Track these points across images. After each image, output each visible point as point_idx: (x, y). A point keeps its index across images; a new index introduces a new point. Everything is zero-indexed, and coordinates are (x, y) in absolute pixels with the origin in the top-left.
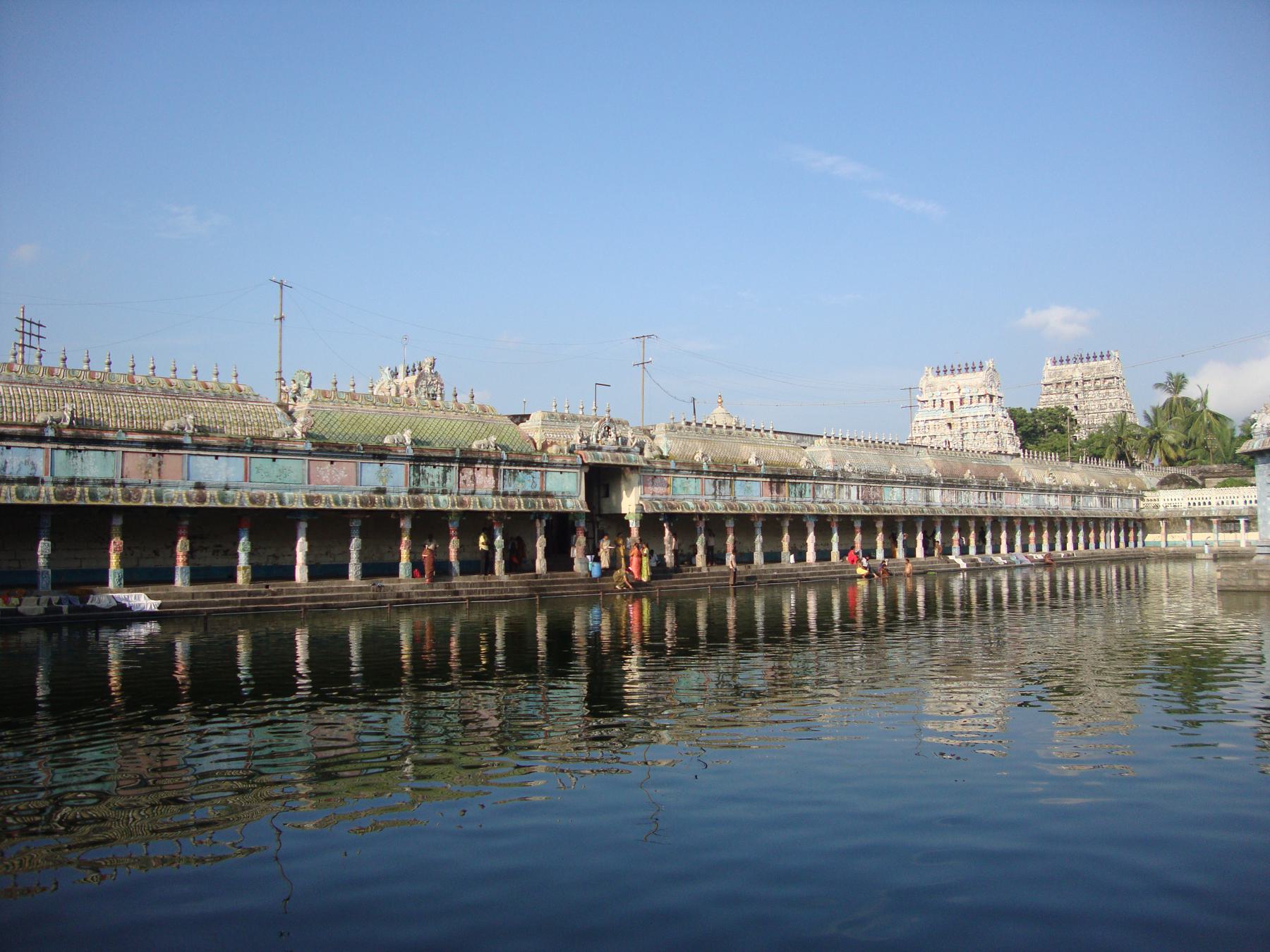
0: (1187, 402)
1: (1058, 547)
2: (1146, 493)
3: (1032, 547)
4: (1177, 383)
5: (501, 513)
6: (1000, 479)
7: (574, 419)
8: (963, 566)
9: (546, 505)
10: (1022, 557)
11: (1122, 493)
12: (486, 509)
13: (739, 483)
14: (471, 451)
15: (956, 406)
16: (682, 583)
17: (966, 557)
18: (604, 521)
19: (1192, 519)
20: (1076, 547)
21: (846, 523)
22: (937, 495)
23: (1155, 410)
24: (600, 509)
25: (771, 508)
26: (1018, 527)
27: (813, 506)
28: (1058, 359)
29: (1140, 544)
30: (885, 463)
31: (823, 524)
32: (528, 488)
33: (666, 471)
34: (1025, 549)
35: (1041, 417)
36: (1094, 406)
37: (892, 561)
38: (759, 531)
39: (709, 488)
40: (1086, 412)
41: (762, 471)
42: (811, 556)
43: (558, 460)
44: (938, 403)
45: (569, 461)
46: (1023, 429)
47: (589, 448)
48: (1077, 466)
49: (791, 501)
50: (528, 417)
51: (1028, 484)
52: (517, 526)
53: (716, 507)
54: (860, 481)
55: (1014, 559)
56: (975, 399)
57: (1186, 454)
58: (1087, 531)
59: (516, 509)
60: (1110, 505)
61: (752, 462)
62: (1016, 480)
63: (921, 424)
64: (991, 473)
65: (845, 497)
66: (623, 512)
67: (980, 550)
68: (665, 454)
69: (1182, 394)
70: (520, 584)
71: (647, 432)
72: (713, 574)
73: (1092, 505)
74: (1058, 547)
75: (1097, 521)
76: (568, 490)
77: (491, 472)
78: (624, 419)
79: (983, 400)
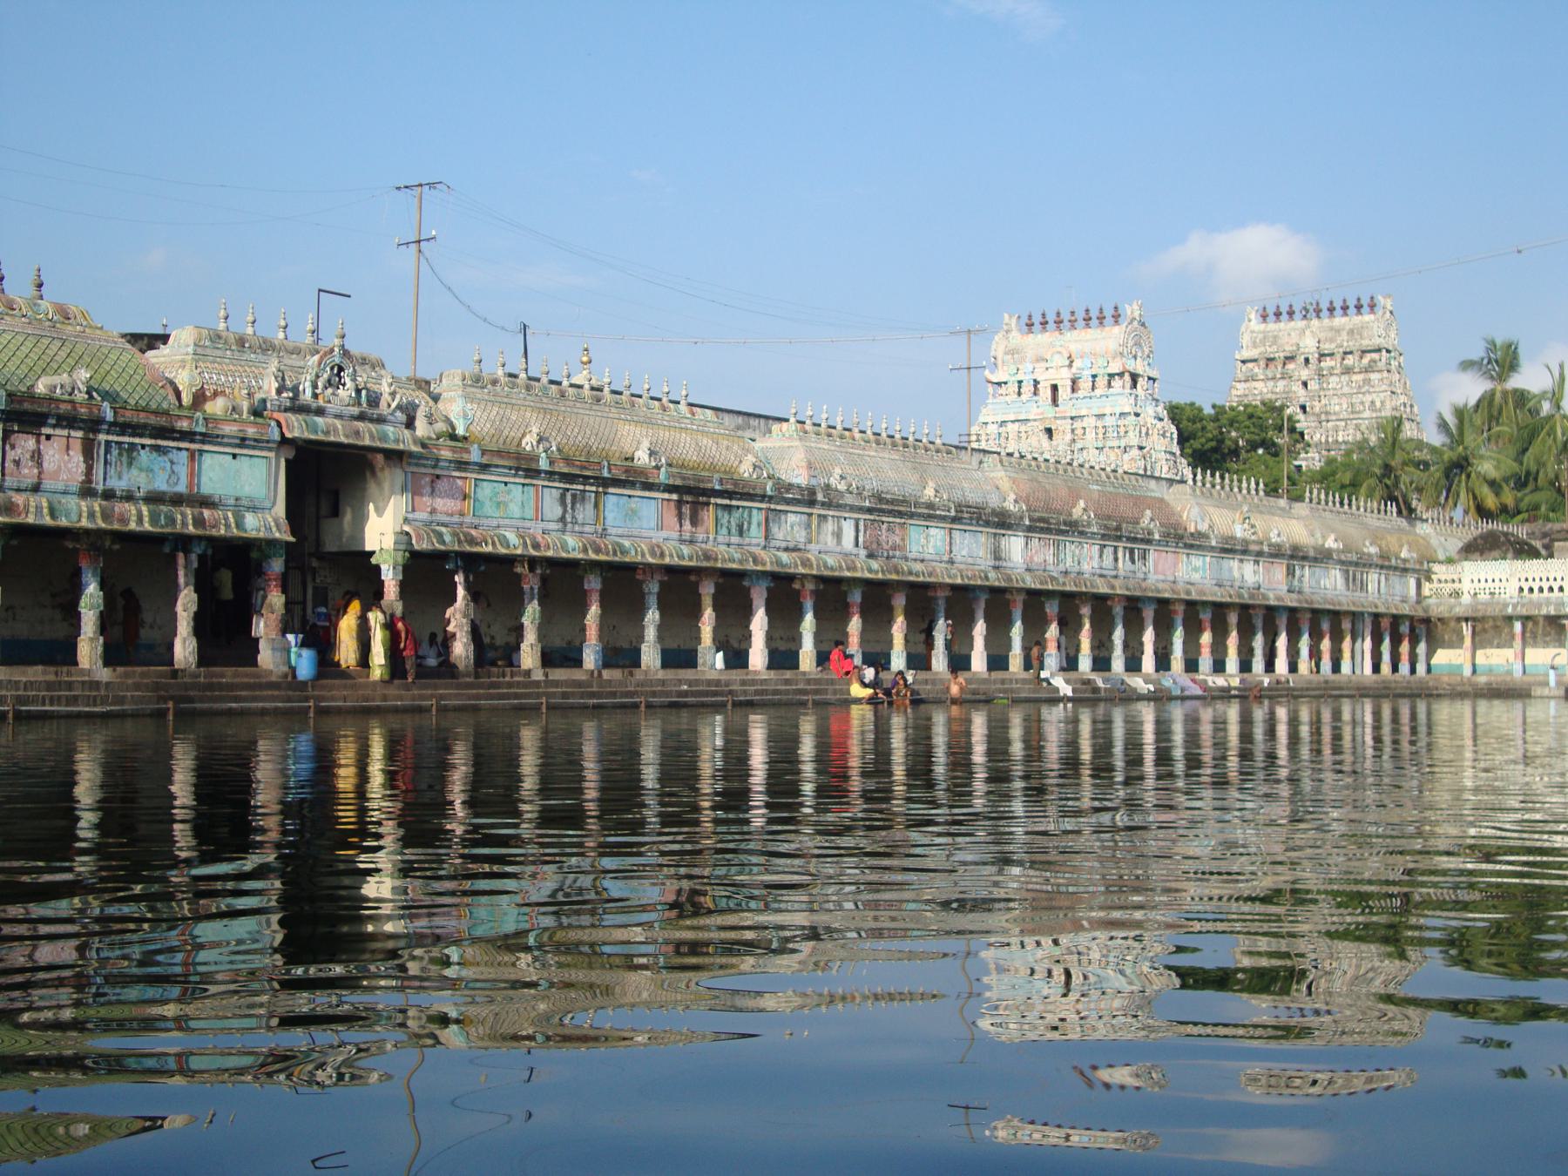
0: (1521, 397)
1: (1258, 664)
2: (1436, 567)
3: (1205, 662)
4: (1504, 360)
5: (100, 533)
6: (1145, 521)
7: (267, 347)
8: (1066, 690)
9: (199, 522)
10: (1185, 680)
11: (1388, 564)
12: (63, 522)
13: (614, 503)
14: (31, 396)
15: (1064, 393)
16: (492, 697)
17: (1072, 675)
18: (326, 572)
19: (1526, 619)
20: (1293, 668)
21: (833, 594)
22: (1016, 548)
23: (1460, 413)
24: (318, 542)
25: (678, 553)
26: (1179, 619)
27: (763, 554)
28: (1271, 311)
29: (1421, 668)
30: (913, 478)
31: (784, 594)
32: (161, 484)
33: (462, 465)
34: (1191, 666)
35: (1232, 423)
36: (1338, 406)
37: (922, 675)
38: (652, 601)
39: (552, 509)
40: (1324, 417)
41: (662, 477)
42: (758, 657)
43: (229, 429)
44: (1027, 388)
45: (251, 431)
46: (1196, 444)
47: (297, 408)
48: (1301, 509)
49: (722, 542)
50: (164, 339)
51: (1200, 535)
52: (138, 563)
53: (564, 547)
54: (861, 509)
55: (1167, 682)
56: (1102, 382)
57: (1518, 501)
58: (1316, 636)
59: (133, 526)
60: (1363, 587)
61: (642, 458)
62: (1176, 526)
63: (992, 429)
64: (1126, 510)
65: (830, 541)
66: (368, 548)
67: (1101, 664)
68: (460, 431)
69: (1516, 382)
70: (137, 687)
71: (423, 384)
72: (556, 683)
73: (1328, 586)
74: (1258, 664)
75: (1335, 616)
76: (248, 493)
77: (77, 446)
78: (374, 354)
79: (1117, 383)
